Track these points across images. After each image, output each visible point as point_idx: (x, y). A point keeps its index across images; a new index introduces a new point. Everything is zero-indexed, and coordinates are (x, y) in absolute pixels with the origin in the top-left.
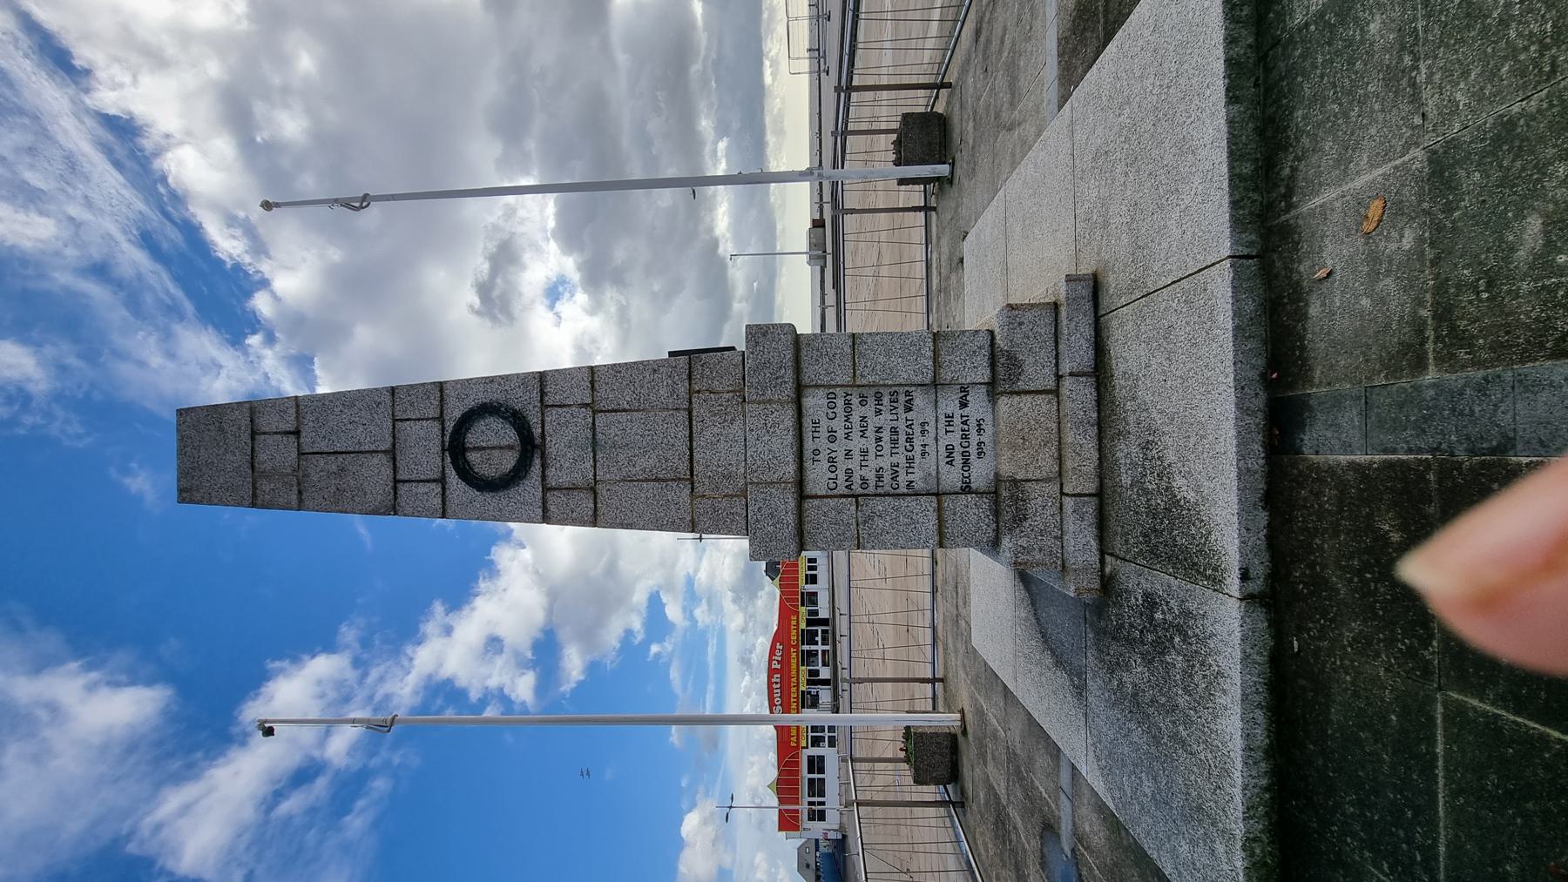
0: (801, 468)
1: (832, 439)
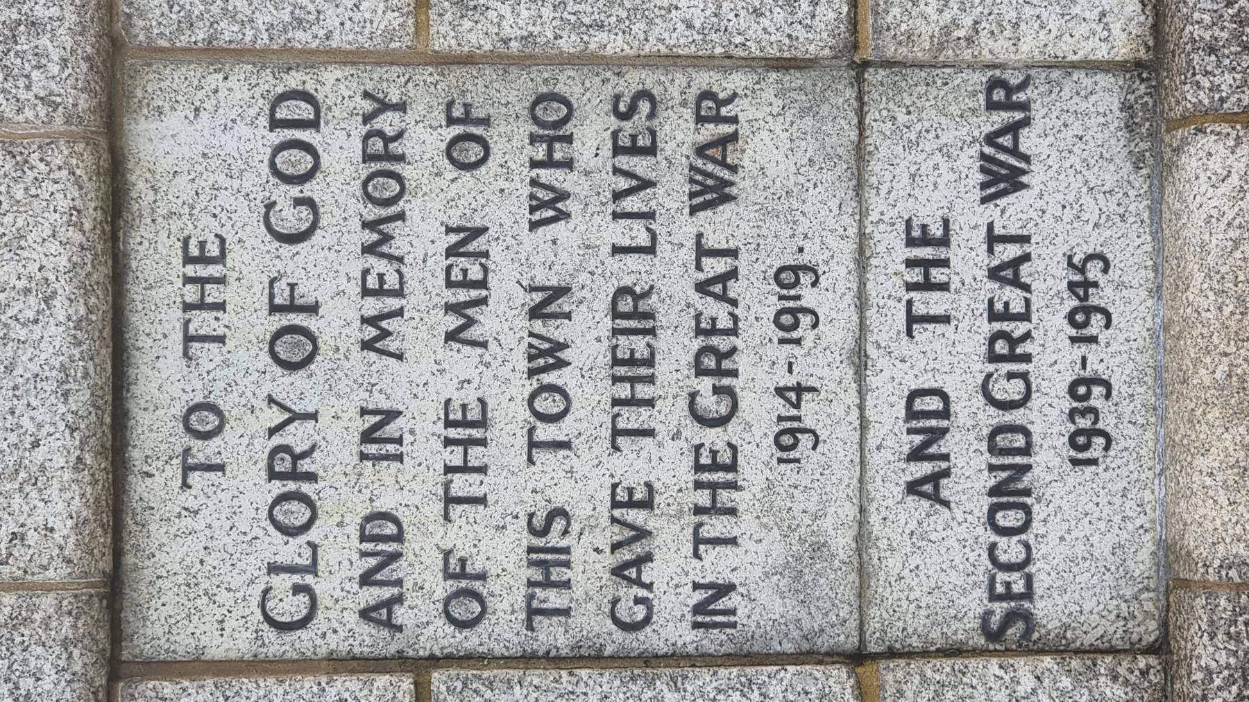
1: (293, 347)
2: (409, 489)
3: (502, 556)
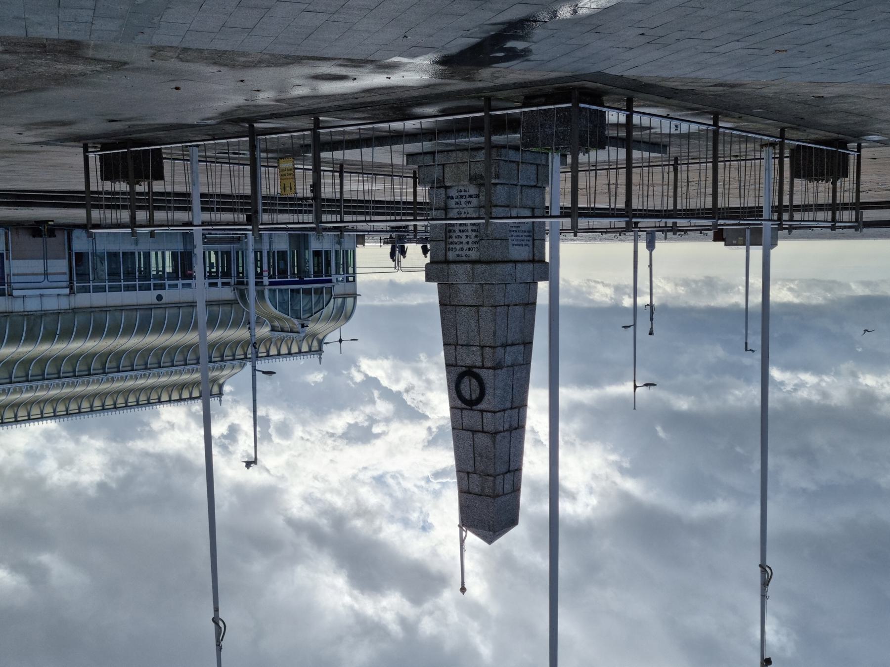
1: (462, 249)
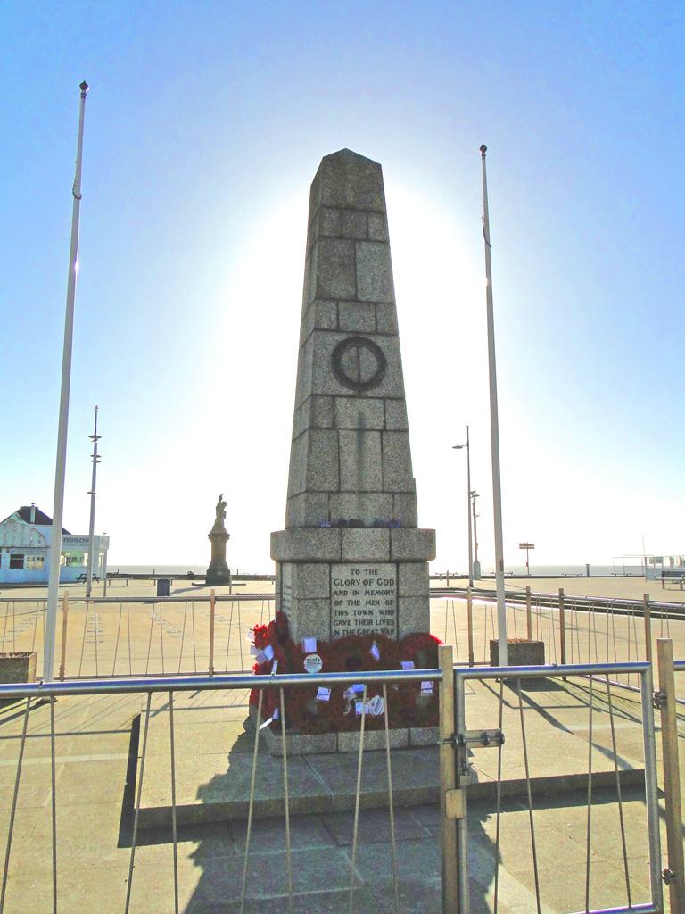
0: (348, 562)
1: (366, 583)
2: (350, 596)
3: (343, 607)
